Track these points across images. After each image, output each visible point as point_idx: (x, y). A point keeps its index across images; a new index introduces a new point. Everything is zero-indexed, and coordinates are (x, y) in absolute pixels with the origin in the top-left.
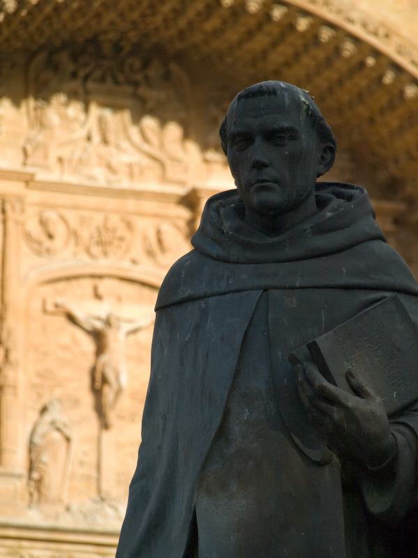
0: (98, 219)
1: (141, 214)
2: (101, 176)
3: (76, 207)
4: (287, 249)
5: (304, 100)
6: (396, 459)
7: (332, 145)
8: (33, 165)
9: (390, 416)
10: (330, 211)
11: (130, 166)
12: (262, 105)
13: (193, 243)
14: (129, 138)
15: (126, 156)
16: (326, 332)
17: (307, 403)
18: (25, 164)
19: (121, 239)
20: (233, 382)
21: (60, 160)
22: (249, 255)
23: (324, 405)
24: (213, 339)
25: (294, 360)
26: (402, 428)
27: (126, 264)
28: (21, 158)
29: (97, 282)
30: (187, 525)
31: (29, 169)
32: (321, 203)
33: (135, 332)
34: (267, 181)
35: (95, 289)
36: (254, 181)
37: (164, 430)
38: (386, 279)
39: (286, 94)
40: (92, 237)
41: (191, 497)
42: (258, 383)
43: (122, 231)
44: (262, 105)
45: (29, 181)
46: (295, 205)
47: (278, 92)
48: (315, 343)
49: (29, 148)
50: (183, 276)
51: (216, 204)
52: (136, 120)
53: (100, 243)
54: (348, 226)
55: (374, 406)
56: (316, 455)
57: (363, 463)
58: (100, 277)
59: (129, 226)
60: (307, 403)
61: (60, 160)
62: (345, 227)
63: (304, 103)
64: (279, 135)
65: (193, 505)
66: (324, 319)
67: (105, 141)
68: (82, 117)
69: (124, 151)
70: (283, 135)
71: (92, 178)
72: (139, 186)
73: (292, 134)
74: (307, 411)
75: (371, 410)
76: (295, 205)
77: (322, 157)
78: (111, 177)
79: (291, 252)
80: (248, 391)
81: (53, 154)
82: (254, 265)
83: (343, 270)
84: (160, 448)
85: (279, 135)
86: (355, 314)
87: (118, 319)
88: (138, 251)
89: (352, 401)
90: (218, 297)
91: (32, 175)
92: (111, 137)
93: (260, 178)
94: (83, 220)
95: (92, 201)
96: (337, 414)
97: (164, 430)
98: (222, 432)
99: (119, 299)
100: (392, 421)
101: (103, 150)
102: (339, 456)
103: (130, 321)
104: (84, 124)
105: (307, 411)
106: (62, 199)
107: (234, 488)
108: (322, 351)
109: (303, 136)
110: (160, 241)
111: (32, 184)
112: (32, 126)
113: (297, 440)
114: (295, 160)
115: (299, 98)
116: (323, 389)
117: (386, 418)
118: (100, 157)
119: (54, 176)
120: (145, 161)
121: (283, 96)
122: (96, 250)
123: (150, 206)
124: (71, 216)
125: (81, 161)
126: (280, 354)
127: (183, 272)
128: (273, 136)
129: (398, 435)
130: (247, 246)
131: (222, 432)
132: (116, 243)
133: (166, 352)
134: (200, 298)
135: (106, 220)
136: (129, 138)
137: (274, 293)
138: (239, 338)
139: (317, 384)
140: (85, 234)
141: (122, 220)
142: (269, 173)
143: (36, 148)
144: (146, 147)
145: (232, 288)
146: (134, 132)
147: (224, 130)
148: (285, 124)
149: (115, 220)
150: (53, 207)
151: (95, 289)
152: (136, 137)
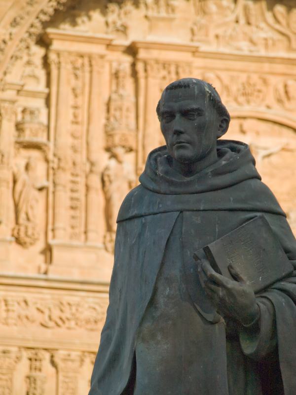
0: (243, 77)
1: (273, 73)
2: (245, 47)
3: (228, 70)
4: (196, 186)
5: (208, 90)
6: (259, 320)
7: (227, 118)
8: (199, 41)
9: (256, 293)
10: (225, 161)
11: (266, 39)
12: (180, 94)
13: (140, 180)
14: (265, 21)
15: (263, 33)
16: (218, 239)
17: (203, 285)
18: (192, 40)
19: (259, 91)
20: (160, 271)
21: (217, 36)
22: (172, 189)
23: (213, 287)
24: (149, 243)
25: (196, 258)
26: (264, 300)
27: (263, 109)
28: (189, 36)
29: (242, 121)
30: (131, 362)
31: (195, 44)
32: (221, 154)
33: (269, 156)
34: (184, 142)
35: (241, 126)
36: (175, 143)
37: (120, 299)
38: (259, 205)
39: (196, 87)
40: (238, 90)
41: (133, 343)
42: (175, 271)
43: (260, 85)
44: (180, 94)
45: (195, 52)
46: (202, 157)
47: (191, 86)
48: (207, 248)
49: (195, 28)
50: (133, 201)
51: (155, 155)
52: (271, 8)
53: (244, 94)
54: (235, 170)
55: (247, 286)
56: (210, 317)
57: (239, 324)
58: (244, 118)
59: (265, 82)
60: (203, 285)
61: (217, 36)
62: (233, 171)
63: (208, 92)
64: (191, 113)
65: (134, 348)
66: (217, 230)
67: (249, 23)
68: (232, 6)
69: (262, 29)
70: (193, 113)
71: (239, 49)
72: (272, 54)
73: (199, 112)
74: (204, 291)
75: (243, 290)
76: (202, 157)
77: (221, 126)
78: (253, 48)
79: (197, 187)
80: (169, 276)
81: (212, 33)
82: (175, 196)
83: (229, 199)
84: (118, 310)
85: (191, 113)
86: (237, 227)
87: (257, 147)
88: (271, 99)
89: (231, 284)
90: (152, 216)
91: (197, 48)
92: (253, 20)
93: (179, 141)
94: (232, 79)
95: (239, 65)
96: (221, 292)
97: (120, 299)
98: (152, 303)
99: (258, 133)
100: (259, 295)
101: (247, 29)
102: (225, 318)
103: (265, 149)
104: (233, 12)
105: (204, 291)
106: (218, 64)
107: (159, 338)
108: (212, 252)
109: (207, 114)
110: (286, 92)
111: (197, 54)
112: (197, 13)
113: (199, 308)
114: (201, 129)
115: (205, 89)
116: (212, 276)
117: (253, 293)
118: (245, 34)
119: (213, 48)
120: (277, 36)
121: (194, 88)
122: (242, 99)
123: (280, 68)
124: (224, 76)
125: (231, 37)
126: (189, 253)
127: (133, 199)
128: (186, 114)
129: (261, 305)
130: (171, 183)
131: (152, 303)
132: (256, 94)
133: (122, 250)
134: (142, 216)
135: (249, 77)
136: (265, 21)
137: (187, 214)
138: (164, 243)
139: (209, 273)
140: (234, 88)
141: (261, 78)
142: (184, 137)
143: (200, 29)
144: (277, 26)
145: (161, 210)
146: (269, 16)
147: (159, 109)
148: (195, 106)
149: (255, 78)
150: (212, 69)
151: (241, 126)
152: (270, 19)
